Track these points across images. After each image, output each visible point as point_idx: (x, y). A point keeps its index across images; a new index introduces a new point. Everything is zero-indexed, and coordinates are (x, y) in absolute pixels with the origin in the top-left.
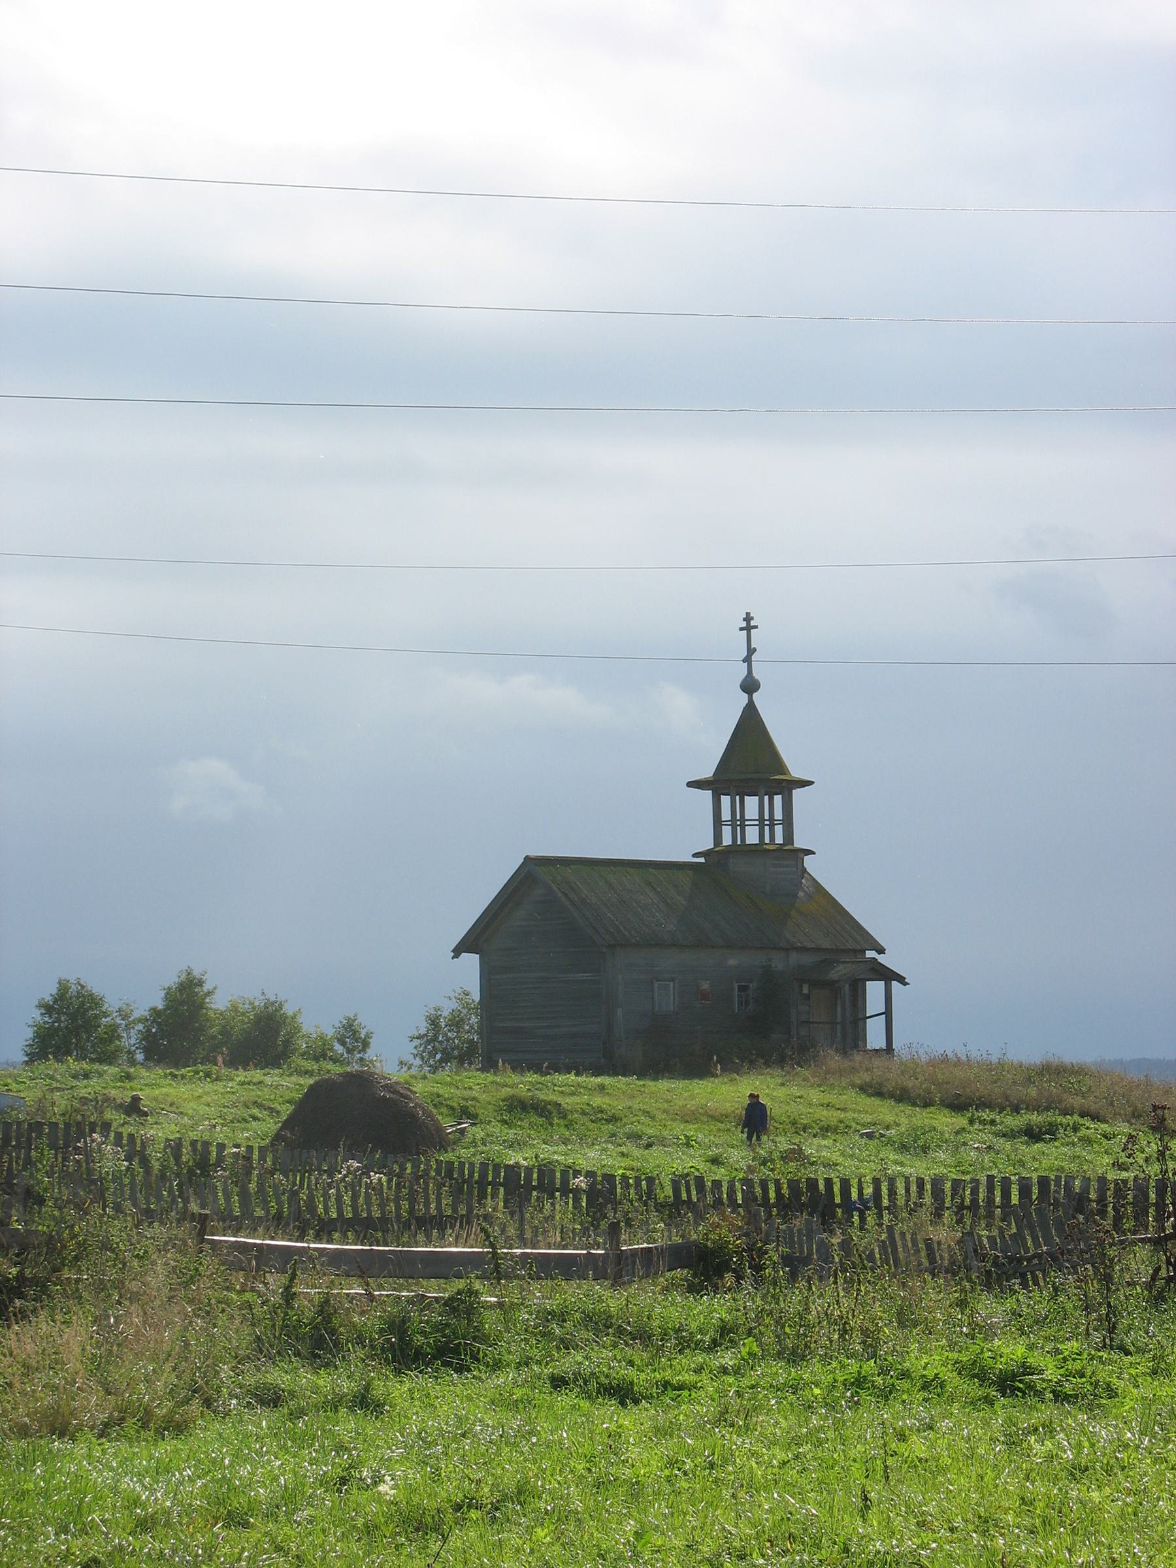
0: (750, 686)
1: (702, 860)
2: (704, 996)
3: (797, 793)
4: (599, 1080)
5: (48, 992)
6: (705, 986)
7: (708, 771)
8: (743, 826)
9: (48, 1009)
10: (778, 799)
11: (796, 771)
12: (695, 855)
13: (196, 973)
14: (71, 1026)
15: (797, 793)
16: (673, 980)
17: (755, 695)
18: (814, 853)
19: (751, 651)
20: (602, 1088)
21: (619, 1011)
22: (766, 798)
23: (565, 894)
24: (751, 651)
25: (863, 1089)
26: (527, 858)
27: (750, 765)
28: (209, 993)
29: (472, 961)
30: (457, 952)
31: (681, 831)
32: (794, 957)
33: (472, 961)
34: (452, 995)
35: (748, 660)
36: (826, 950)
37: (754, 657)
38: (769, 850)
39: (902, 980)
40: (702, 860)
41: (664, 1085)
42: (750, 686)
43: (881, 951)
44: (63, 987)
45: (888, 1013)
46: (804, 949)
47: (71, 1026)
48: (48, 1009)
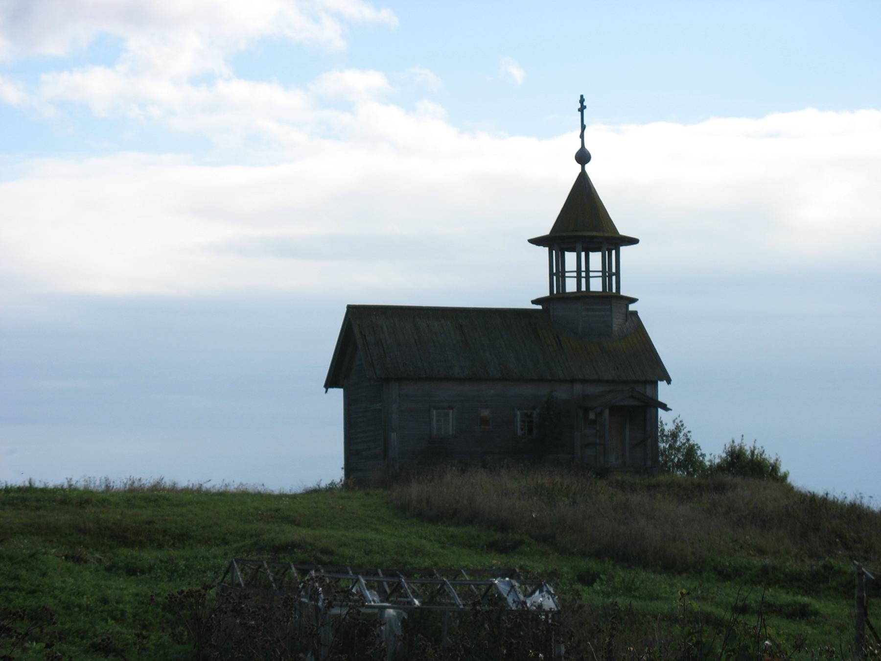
0: (583, 157)
1: (540, 307)
2: (484, 421)
3: (623, 249)
6: (485, 413)
7: (546, 229)
8: (588, 278)
10: (614, 252)
12: (534, 302)
15: (623, 249)
16: (451, 408)
17: (588, 167)
21: (394, 435)
22: (583, 254)
27: (582, 224)
28: (753, 452)
29: (338, 394)
31: (518, 280)
32: (578, 388)
33: (338, 394)
36: (607, 382)
40: (540, 307)
42: (583, 157)
46: (584, 381)
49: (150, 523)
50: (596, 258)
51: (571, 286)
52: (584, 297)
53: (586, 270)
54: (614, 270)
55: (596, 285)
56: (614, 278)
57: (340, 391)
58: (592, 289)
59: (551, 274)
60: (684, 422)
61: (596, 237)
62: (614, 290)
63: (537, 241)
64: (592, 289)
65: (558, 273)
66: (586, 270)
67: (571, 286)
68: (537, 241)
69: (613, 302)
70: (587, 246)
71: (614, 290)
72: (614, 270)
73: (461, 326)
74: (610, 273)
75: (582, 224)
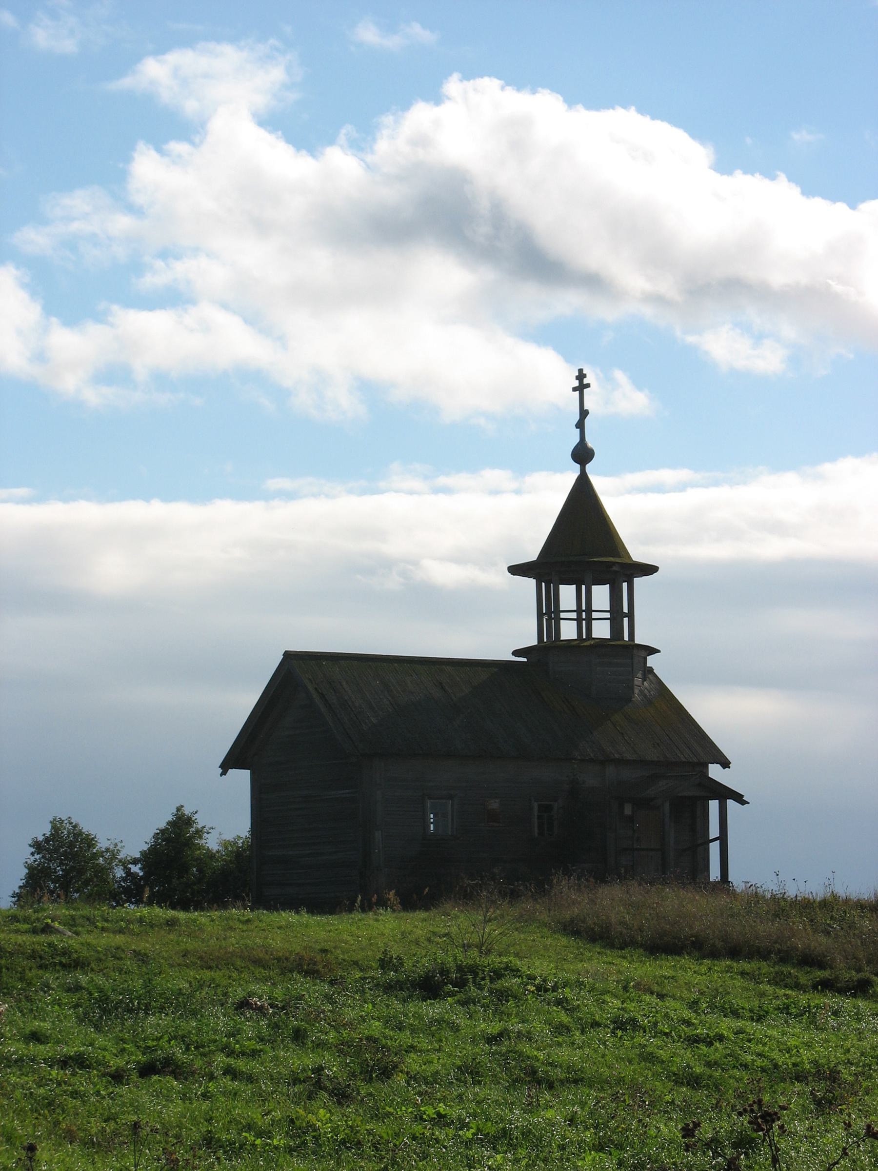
0: (582, 455)
4: (171, 913)
5: (43, 830)
6: (494, 805)
7: (532, 552)
9: (38, 846)
11: (637, 553)
13: (187, 811)
14: (65, 864)
17: (589, 467)
18: (659, 651)
19: (584, 413)
20: (172, 923)
21: (378, 835)
23: (322, 696)
24: (584, 413)
25: (572, 929)
26: (288, 655)
27: (583, 547)
29: (242, 778)
30: (226, 765)
31: (501, 627)
33: (242, 778)
34: (196, 816)
35: (580, 425)
37: (577, 418)
38: (574, 646)
39: (739, 798)
41: (287, 917)
42: (582, 455)
43: (726, 764)
44: (56, 826)
45: (723, 838)
46: (622, 762)
47: (65, 864)
48: (38, 846)
49: (324, 951)
50: (601, 595)
51: (568, 631)
52: (585, 645)
53: (585, 610)
54: (626, 610)
55: (601, 630)
56: (626, 620)
57: (246, 773)
58: (596, 634)
59: (631, 615)
60: (74, 821)
61: (614, 563)
62: (626, 638)
63: (516, 570)
64: (596, 634)
65: (548, 613)
66: (585, 610)
67: (568, 631)
68: (516, 570)
69: (626, 655)
70: (584, 578)
71: (626, 638)
72: (626, 610)
73: (441, 684)
74: (618, 614)
75: (583, 547)
